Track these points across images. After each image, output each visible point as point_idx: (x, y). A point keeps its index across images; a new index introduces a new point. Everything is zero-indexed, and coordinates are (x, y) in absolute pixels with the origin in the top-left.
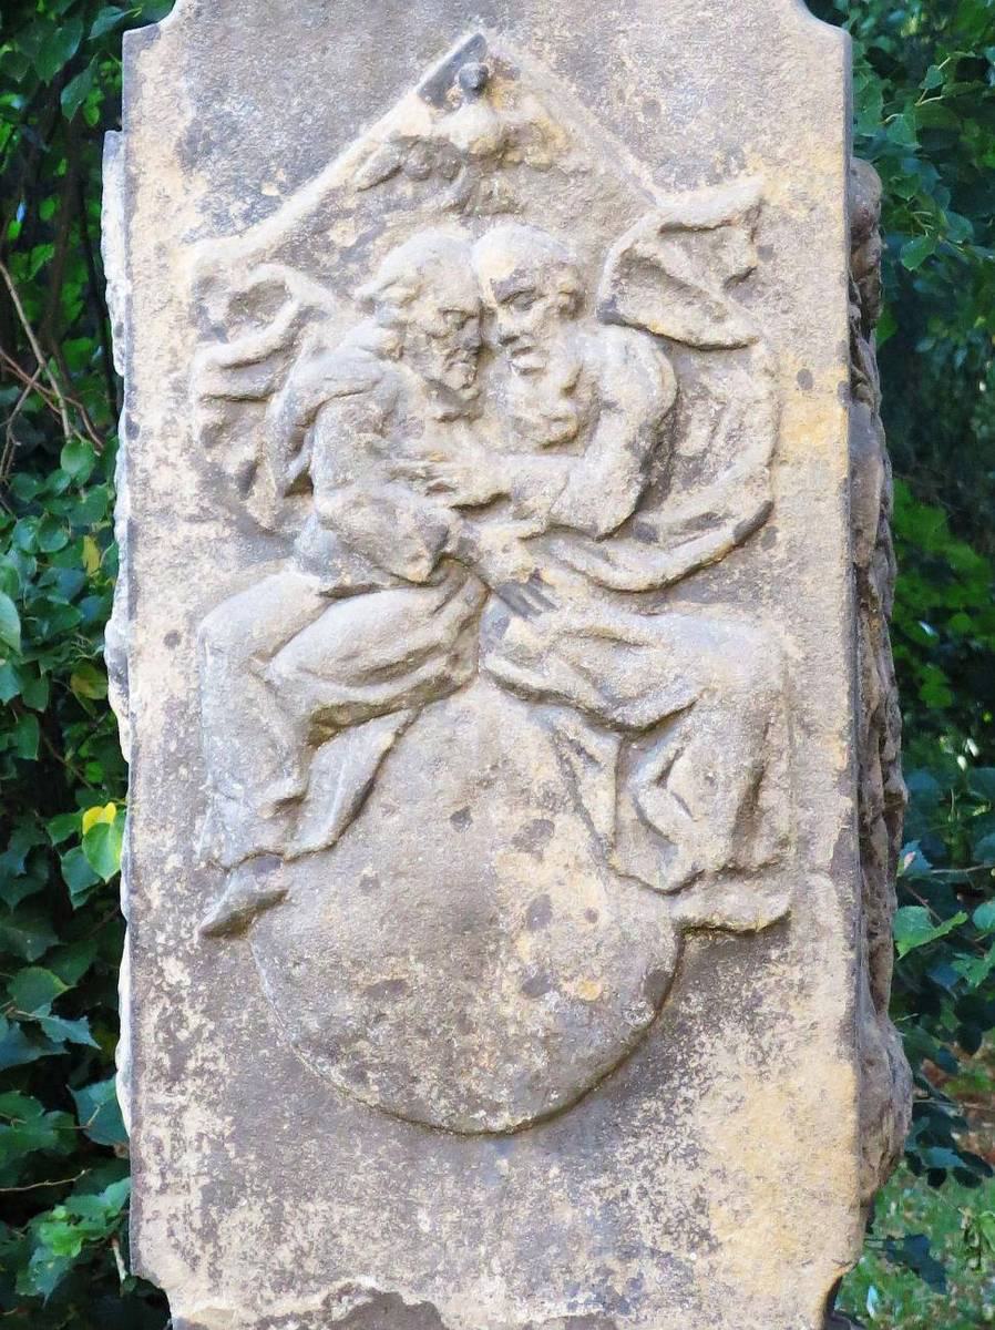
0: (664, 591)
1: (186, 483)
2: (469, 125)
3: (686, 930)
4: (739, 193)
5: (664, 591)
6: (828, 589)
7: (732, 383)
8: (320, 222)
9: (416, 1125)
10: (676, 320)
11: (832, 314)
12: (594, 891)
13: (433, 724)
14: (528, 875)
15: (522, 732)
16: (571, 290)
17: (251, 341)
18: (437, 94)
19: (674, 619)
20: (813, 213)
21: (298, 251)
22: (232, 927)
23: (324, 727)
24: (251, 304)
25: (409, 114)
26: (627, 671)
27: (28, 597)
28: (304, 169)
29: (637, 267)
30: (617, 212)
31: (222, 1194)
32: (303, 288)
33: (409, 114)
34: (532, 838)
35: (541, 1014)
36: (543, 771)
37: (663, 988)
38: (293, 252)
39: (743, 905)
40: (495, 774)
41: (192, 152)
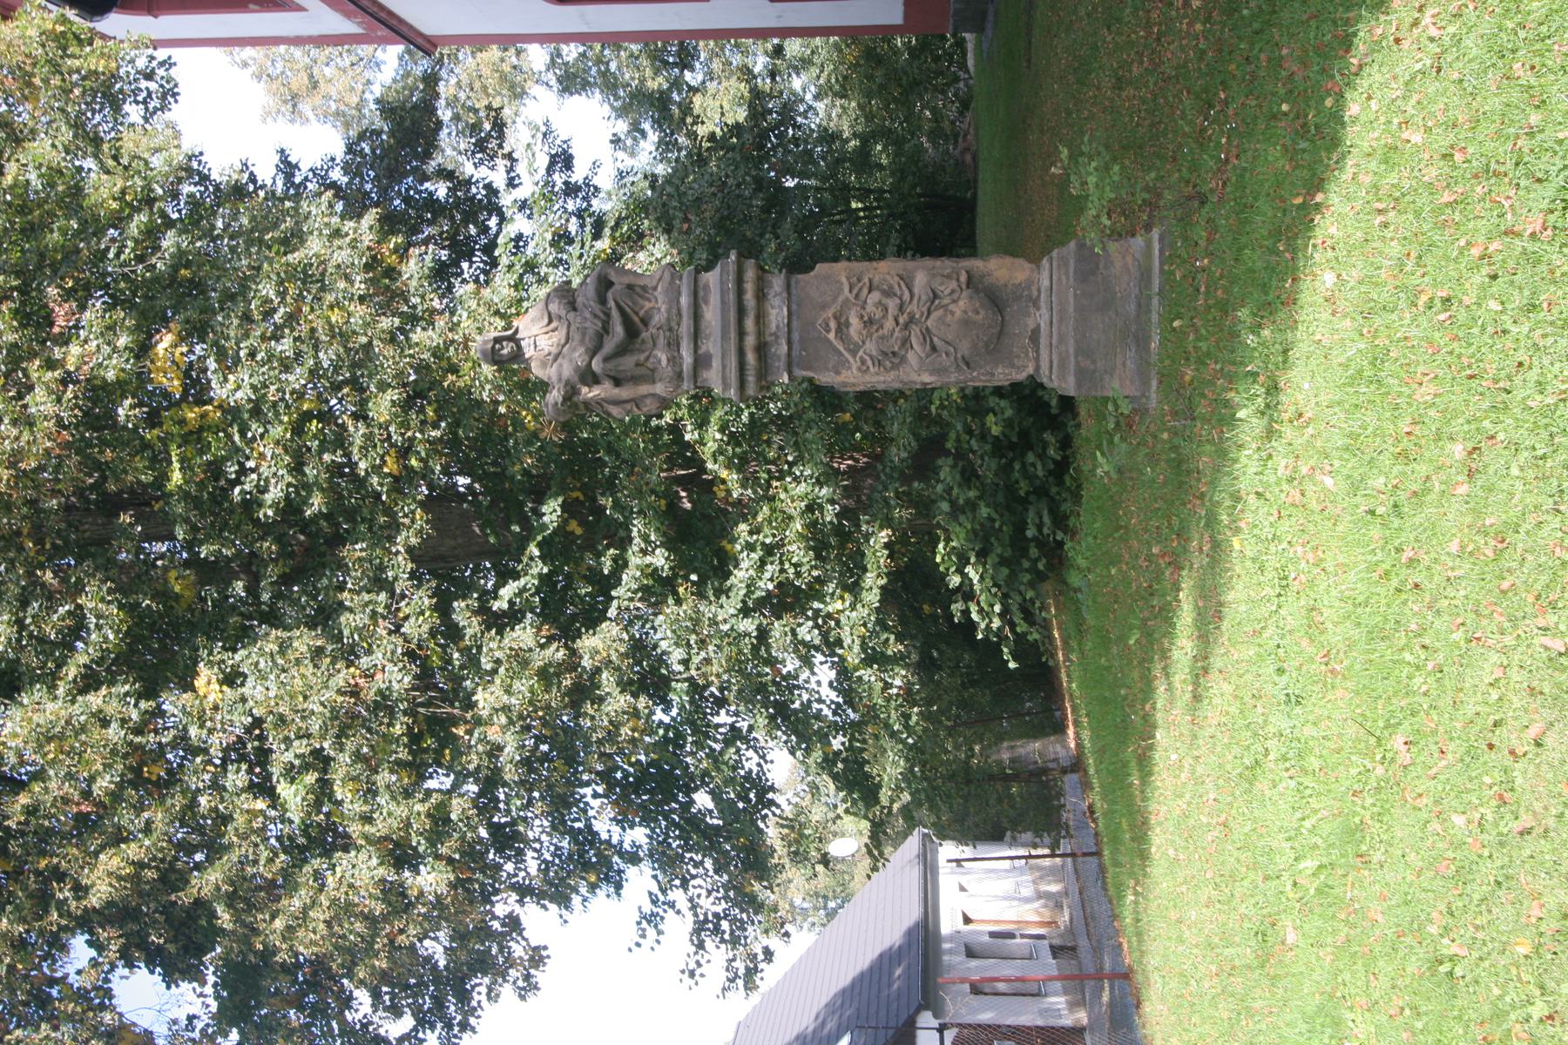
0: (911, 291)
1: (893, 373)
2: (833, 325)
3: (968, 287)
4: (844, 280)
5: (911, 291)
6: (910, 265)
7: (876, 280)
8: (849, 350)
9: (1001, 333)
10: (865, 291)
11: (866, 264)
12: (961, 303)
13: (934, 331)
14: (958, 313)
15: (935, 315)
16: (293, 159)
17: (869, 363)
18: (828, 331)
19: (916, 291)
20: (1519, 752)
21: (854, 353)
22: (968, 364)
23: (934, 348)
24: (863, 362)
25: (831, 336)
26: (924, 298)
27: (813, 924)
28: (840, 354)
29: (857, 297)
30: (847, 300)
31: (1013, 366)
32: (861, 353)
33: (831, 336)
34: (952, 313)
35: (982, 312)
36: (940, 312)
37: (977, 291)
38: (854, 356)
39: (963, 278)
40: (941, 320)
41: (838, 373)
